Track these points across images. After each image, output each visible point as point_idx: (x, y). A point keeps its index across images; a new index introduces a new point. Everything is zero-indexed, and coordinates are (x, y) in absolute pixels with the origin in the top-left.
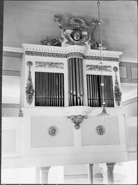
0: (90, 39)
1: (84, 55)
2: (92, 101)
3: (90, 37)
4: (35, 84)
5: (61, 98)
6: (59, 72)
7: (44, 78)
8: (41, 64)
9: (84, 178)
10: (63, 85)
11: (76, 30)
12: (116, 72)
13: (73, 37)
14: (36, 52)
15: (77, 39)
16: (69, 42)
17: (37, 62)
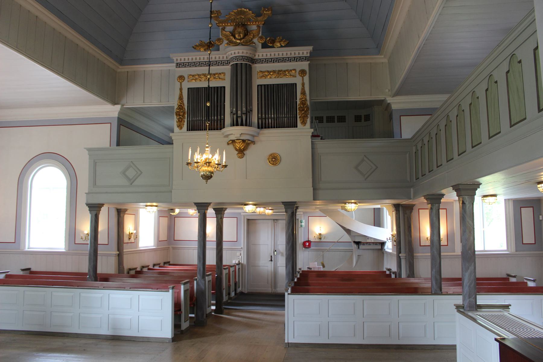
0: (260, 35)
1: (254, 58)
3: (261, 32)
4: (188, 104)
7: (193, 97)
8: (194, 77)
9: (448, 281)
10: (224, 102)
11: (237, 26)
14: (199, 62)
15: (239, 38)
16: (230, 43)
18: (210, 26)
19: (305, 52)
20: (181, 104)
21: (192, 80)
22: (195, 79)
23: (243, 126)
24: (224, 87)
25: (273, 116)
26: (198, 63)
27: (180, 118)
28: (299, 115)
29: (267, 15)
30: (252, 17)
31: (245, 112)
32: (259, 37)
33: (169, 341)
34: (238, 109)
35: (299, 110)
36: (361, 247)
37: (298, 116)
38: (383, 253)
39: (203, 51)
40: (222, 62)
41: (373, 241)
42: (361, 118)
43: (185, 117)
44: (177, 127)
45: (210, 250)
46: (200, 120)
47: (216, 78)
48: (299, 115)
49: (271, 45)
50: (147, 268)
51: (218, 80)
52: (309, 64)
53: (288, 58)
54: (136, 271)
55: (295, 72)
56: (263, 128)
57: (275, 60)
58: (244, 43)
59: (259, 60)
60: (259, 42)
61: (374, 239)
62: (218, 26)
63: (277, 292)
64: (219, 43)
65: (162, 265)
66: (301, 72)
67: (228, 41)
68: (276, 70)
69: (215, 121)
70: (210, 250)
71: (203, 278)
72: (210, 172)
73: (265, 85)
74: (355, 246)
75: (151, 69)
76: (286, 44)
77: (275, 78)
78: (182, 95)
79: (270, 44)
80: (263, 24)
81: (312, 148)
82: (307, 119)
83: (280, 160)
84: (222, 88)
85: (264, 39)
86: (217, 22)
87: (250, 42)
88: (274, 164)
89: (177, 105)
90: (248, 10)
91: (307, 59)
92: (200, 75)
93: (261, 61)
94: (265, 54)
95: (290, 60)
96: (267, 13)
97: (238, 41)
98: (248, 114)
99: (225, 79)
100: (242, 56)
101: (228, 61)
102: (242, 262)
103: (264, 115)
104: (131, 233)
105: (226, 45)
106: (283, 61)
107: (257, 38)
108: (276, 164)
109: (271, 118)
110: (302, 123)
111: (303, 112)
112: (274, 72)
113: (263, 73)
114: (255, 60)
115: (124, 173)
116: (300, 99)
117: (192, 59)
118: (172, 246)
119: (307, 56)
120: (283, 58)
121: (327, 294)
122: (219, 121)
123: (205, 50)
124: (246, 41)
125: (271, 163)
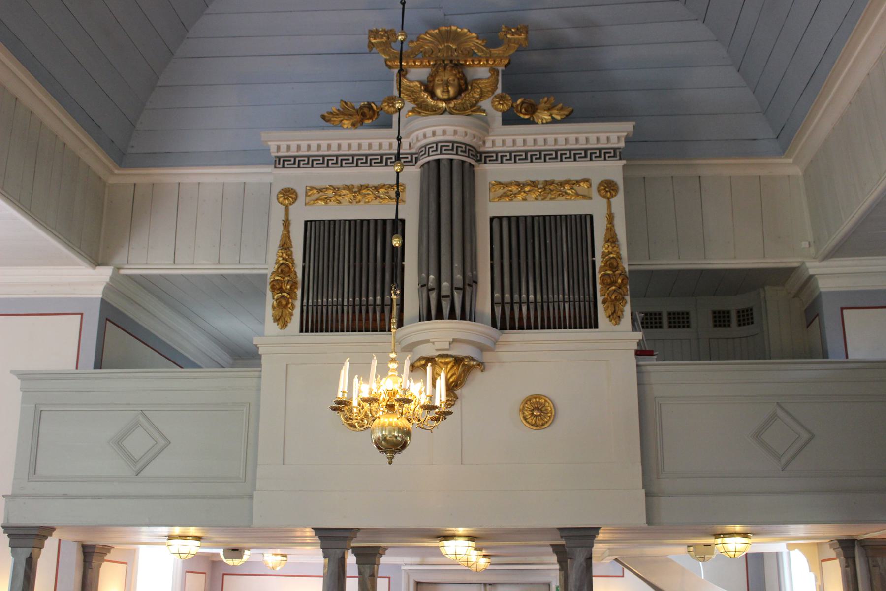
0: (499, 91)
1: (482, 149)
2: (507, 309)
4: (304, 261)
5: (584, 299)
6: (324, 219)
8: (321, 193)
10: (403, 260)
11: (439, 65)
12: (612, 200)
13: (433, 95)
16: (422, 109)
17: (312, 188)
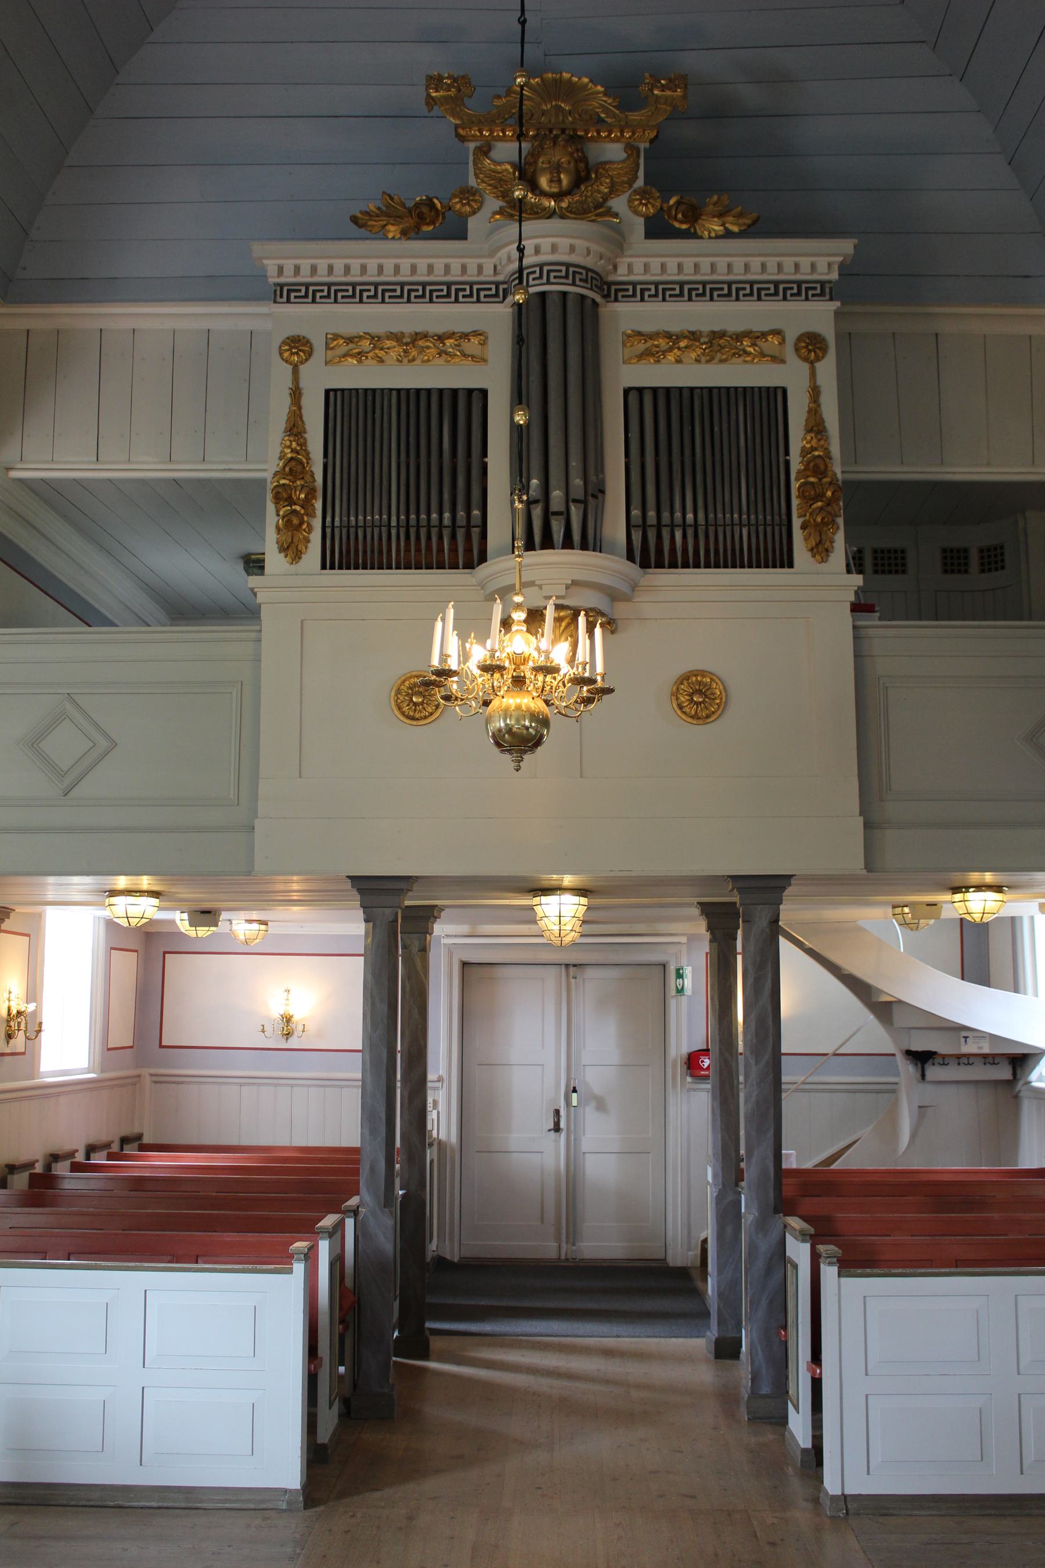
0: (640, 182)
1: (612, 278)
3: (641, 173)
4: (326, 455)
10: (485, 454)
15: (555, 190)
18: (519, 80)
19: (822, 263)
20: (298, 453)
21: (344, 356)
22: (359, 353)
23: (572, 548)
24: (484, 393)
25: (690, 516)
26: (372, 288)
27: (294, 511)
28: (799, 517)
29: (665, 104)
30: (606, 111)
31: (580, 496)
32: (635, 191)
33: (289, 1503)
34: (553, 481)
35: (802, 495)
36: (934, 1072)
37: (797, 522)
38: (1016, 1097)
39: (398, 236)
40: (475, 287)
41: (986, 1050)
42: (966, 558)
43: (314, 509)
44: (280, 552)
45: (309, 1086)
46: (380, 526)
47: (446, 353)
48: (799, 517)
49: (684, 227)
50: (67, 1164)
51: (457, 360)
52: (837, 314)
53: (752, 283)
54: (32, 1175)
55: (780, 344)
56: (650, 567)
57: (698, 289)
58: (571, 212)
59: (631, 288)
60: (636, 213)
61: (994, 1038)
62: (462, 139)
63: (579, 1257)
64: (468, 209)
65: (115, 1148)
66: (808, 344)
67: (507, 202)
68: (702, 329)
69: (446, 533)
70: (309, 1086)
71: (385, 1206)
72: (534, 716)
73: (655, 390)
74: (907, 1069)
75: (131, 324)
76: (745, 224)
77: (698, 361)
78: (301, 418)
79: (682, 222)
80: (652, 141)
81: (856, 656)
82: (834, 534)
83: (726, 702)
84: (475, 394)
85: (655, 199)
86: (458, 122)
87: (596, 207)
88: (699, 718)
89: (280, 459)
90: (586, 80)
91: (827, 290)
92: (379, 338)
93: (638, 292)
94: (655, 263)
95: (756, 291)
96: (666, 98)
97: (547, 204)
98: (591, 501)
99: (484, 360)
100: (568, 265)
101: (497, 284)
102: (443, 1136)
103: (652, 514)
104: (14, 1012)
105: (498, 216)
106: (729, 294)
107: (626, 196)
108: (708, 717)
109: (684, 526)
110: (812, 550)
111: (819, 504)
112: (694, 336)
113: (646, 341)
114: (613, 288)
115: (34, 743)
116: (804, 452)
117: (347, 269)
118: (153, 1071)
119: (829, 282)
120: (730, 284)
121: (953, 1270)
122: (460, 534)
123: (405, 234)
124: (582, 203)
125: (687, 710)
